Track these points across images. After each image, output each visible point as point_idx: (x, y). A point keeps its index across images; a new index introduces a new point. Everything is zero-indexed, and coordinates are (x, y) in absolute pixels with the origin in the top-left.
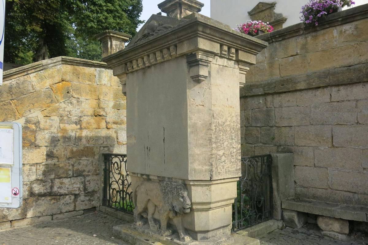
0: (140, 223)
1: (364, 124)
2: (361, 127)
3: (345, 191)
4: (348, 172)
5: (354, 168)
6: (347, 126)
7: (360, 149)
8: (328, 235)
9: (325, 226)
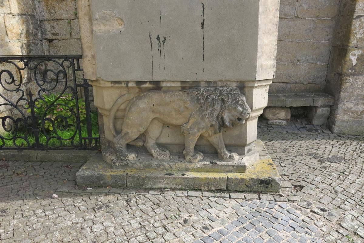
0: (133, 155)
1: (302, 18)
2: (299, 20)
3: (280, 83)
4: (284, 65)
5: (289, 60)
6: (287, 20)
7: (296, 42)
8: (275, 123)
9: (273, 116)
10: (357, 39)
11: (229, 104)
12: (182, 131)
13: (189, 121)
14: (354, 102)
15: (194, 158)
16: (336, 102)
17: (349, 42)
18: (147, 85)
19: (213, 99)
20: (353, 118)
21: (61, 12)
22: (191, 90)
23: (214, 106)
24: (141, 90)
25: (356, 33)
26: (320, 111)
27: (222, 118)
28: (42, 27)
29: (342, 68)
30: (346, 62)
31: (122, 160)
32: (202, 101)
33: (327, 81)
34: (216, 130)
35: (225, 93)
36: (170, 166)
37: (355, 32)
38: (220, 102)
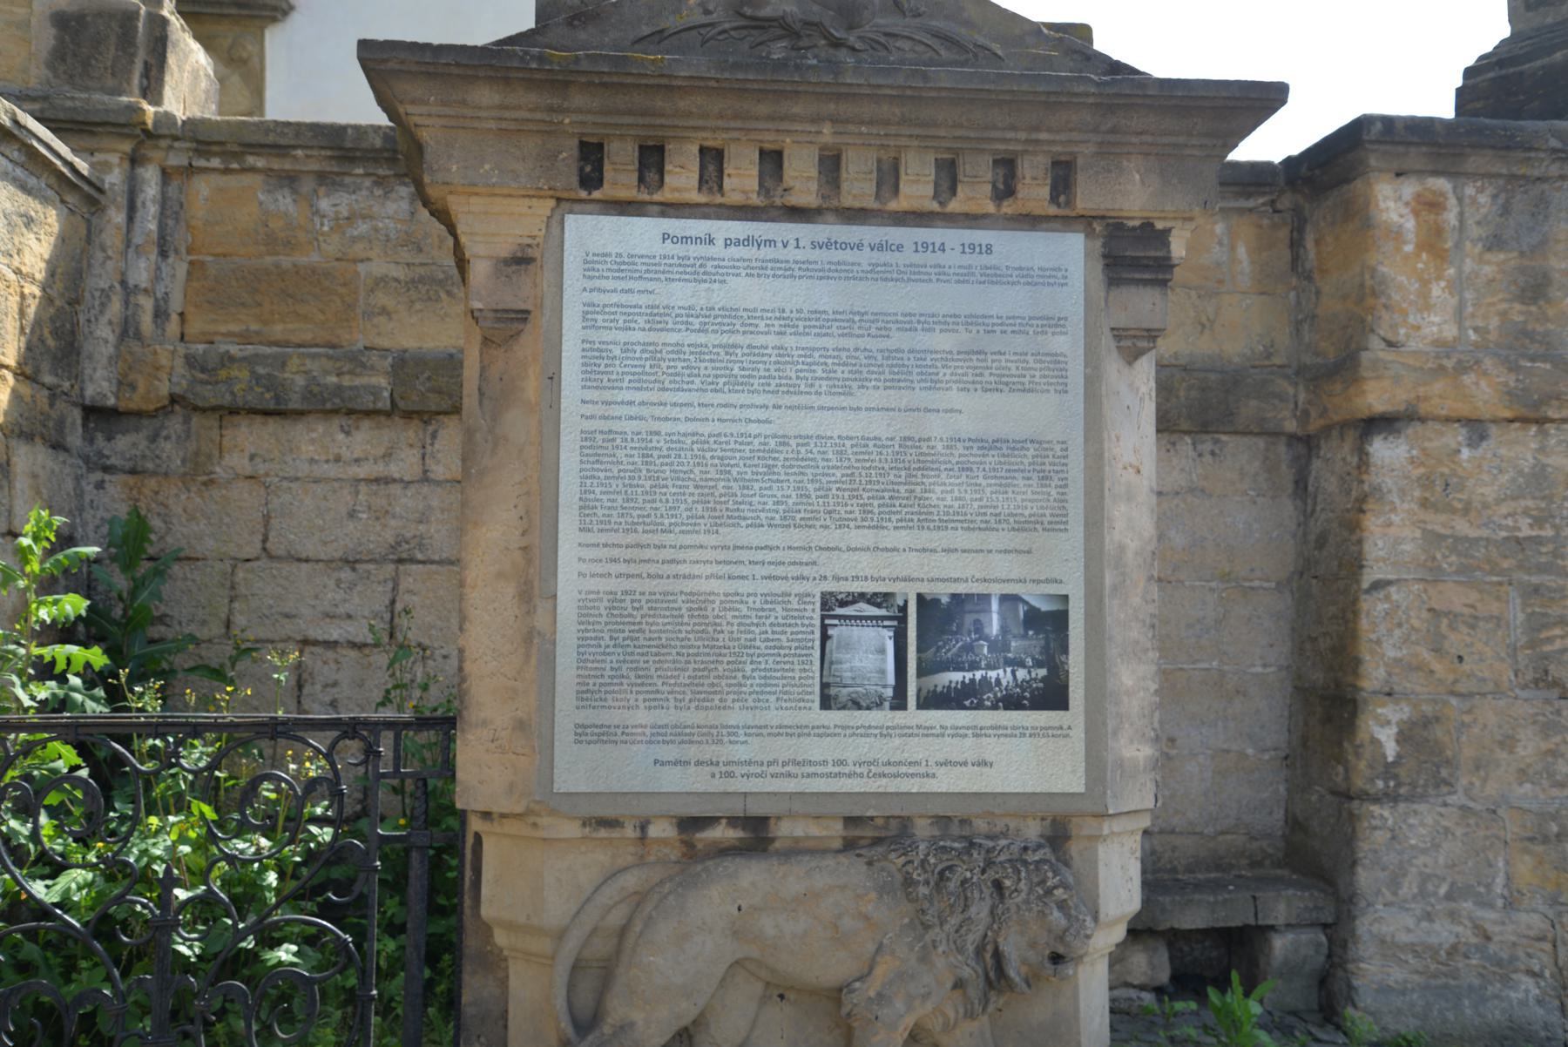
10: (1386, 665)
11: (1019, 900)
12: (845, 1010)
13: (871, 969)
14: (1417, 908)
17: (1355, 673)
18: (721, 833)
19: (964, 882)
20: (1421, 973)
21: (196, 528)
22: (881, 849)
23: (966, 908)
24: (691, 853)
25: (1378, 642)
26: (1280, 944)
27: (997, 955)
28: (95, 589)
29: (1347, 770)
30: (1361, 750)
32: (923, 890)
33: (1295, 824)
34: (972, 1004)
37: (1373, 637)
38: (987, 892)
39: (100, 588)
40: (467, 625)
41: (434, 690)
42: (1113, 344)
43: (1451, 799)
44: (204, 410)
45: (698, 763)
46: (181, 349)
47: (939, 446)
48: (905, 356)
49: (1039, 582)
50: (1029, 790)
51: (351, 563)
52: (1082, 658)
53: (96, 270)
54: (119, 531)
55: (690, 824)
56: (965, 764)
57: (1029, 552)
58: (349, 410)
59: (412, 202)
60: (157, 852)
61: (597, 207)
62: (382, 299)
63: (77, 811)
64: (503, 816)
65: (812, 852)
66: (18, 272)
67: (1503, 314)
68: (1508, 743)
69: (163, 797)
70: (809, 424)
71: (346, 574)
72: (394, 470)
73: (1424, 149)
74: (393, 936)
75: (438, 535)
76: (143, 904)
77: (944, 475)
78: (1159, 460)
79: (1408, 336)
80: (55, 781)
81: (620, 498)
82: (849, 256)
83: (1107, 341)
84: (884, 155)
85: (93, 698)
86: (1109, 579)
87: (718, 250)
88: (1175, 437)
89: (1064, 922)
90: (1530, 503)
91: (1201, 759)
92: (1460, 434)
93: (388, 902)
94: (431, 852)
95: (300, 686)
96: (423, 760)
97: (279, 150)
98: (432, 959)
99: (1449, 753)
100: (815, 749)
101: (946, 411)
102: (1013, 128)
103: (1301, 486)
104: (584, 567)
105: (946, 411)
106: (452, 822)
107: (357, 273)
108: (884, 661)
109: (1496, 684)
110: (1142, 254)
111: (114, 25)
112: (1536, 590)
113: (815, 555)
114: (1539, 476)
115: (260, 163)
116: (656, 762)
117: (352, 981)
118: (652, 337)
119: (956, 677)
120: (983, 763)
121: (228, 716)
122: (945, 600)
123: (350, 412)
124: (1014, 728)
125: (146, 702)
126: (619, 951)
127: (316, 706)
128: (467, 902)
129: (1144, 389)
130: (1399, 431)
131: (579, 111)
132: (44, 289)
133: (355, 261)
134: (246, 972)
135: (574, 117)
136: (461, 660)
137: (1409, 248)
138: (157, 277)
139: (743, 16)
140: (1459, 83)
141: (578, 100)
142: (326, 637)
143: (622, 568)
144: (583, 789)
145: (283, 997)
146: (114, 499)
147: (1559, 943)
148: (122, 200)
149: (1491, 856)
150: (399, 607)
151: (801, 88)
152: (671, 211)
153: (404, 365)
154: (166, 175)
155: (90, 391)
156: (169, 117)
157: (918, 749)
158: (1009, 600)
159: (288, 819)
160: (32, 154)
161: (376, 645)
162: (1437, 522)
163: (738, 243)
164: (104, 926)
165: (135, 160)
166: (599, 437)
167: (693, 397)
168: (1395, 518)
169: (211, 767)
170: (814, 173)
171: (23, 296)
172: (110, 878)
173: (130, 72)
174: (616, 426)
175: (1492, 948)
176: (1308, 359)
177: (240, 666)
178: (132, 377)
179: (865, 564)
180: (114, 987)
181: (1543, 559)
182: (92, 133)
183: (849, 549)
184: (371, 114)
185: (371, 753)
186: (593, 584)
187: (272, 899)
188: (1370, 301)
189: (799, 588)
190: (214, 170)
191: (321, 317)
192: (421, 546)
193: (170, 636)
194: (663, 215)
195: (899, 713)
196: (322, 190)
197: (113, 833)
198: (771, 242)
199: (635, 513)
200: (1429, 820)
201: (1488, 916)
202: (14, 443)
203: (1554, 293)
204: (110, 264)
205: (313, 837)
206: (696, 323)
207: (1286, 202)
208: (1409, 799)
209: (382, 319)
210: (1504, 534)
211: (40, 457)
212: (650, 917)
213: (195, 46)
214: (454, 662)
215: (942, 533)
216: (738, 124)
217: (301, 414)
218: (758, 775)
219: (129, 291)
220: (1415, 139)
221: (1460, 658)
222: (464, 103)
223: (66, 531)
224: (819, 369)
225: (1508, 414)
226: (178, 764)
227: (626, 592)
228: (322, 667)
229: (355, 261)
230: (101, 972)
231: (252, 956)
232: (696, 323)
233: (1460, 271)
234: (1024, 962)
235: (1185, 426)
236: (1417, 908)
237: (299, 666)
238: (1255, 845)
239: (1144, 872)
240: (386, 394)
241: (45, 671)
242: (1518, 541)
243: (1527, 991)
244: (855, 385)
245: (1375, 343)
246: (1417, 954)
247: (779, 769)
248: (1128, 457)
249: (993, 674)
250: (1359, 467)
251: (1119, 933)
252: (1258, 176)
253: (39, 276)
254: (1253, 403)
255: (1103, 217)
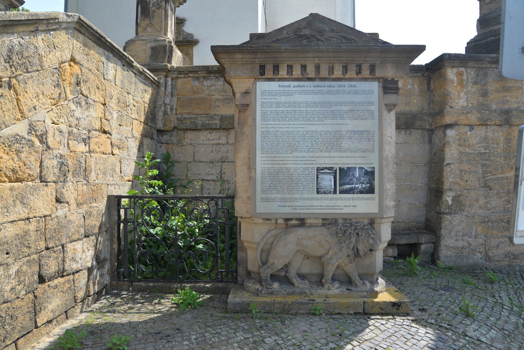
10: (450, 183)
12: (322, 261)
15: (332, 286)
16: (438, 239)
17: (442, 185)
18: (294, 222)
19: (350, 233)
22: (330, 226)
23: (350, 239)
24: (287, 226)
25: (448, 178)
26: (423, 247)
27: (357, 249)
29: (440, 207)
31: (267, 288)
33: (427, 220)
35: (359, 228)
36: (312, 293)
37: (447, 176)
38: (355, 235)
39: (161, 169)
40: (236, 176)
41: (230, 190)
42: (385, 108)
43: (463, 214)
44: (181, 130)
45: (289, 206)
46: (176, 117)
47: (344, 133)
48: (336, 112)
49: (368, 164)
50: (365, 212)
51: (212, 162)
52: (378, 182)
53: (159, 101)
54: (164, 156)
55: (287, 220)
56: (350, 206)
57: (365, 157)
58: (211, 129)
59: (224, 82)
60: (174, 224)
61: (264, 80)
62: (217, 104)
63: (158, 215)
64: (245, 218)
65: (315, 226)
66: (144, 102)
67: (477, 100)
68: (477, 200)
69: (175, 213)
70: (313, 128)
71: (211, 165)
72: (221, 142)
73: (458, 61)
74: (223, 244)
75: (230, 155)
76: (172, 235)
77: (345, 139)
78: (396, 136)
79: (455, 105)
80: (154, 209)
81: (270, 146)
82: (322, 89)
83: (384, 107)
84: (330, 65)
85: (160, 192)
86: (384, 163)
87: (292, 88)
88: (400, 130)
89: (373, 242)
90: (484, 144)
91: (406, 205)
92: (468, 128)
93: (222, 236)
94: (230, 226)
95: (202, 190)
96: (228, 206)
97: (195, 72)
98: (231, 248)
99: (464, 203)
100: (315, 203)
101: (346, 124)
102: (360, 57)
103: (430, 141)
104: (262, 162)
105: (346, 124)
106: (235, 219)
107: (212, 98)
108: (331, 183)
109: (475, 187)
110: (391, 86)
111: (162, 48)
112: (485, 165)
113: (315, 159)
114: (486, 138)
115: (192, 75)
116: (279, 206)
117: (215, 253)
118: (277, 109)
119: (348, 186)
120: (354, 206)
121: (187, 196)
122: (345, 169)
123: (211, 129)
124: (362, 198)
125: (170, 192)
126: (271, 248)
127: (205, 194)
128: (238, 236)
129: (392, 118)
130: (453, 128)
131: (259, 58)
132: (149, 105)
133: (211, 95)
134: (193, 249)
135: (258, 60)
136: (235, 183)
137: (455, 84)
138: (171, 101)
139: (297, 35)
140: (466, 46)
141: (259, 56)
142: (207, 179)
143: (270, 162)
144: (263, 212)
145: (200, 255)
146: (163, 150)
147: (486, 246)
148: (164, 85)
149: (472, 226)
150: (222, 172)
151: (310, 50)
152: (281, 80)
153: (223, 118)
154: (172, 79)
155: (158, 127)
156: (173, 67)
157: (339, 203)
158: (361, 168)
159: (200, 218)
160: (146, 77)
161: (218, 181)
162: (462, 149)
163: (296, 87)
164: (165, 239)
165: (166, 77)
166: (265, 132)
167: (287, 123)
168: (452, 149)
169: (184, 206)
170: (314, 70)
171: (145, 107)
172: (165, 229)
173: (165, 58)
174: (269, 130)
175: (471, 247)
176: (432, 111)
177: (189, 185)
178: (166, 123)
179: (327, 160)
180: (167, 251)
181: (486, 158)
182: (158, 71)
183: (323, 157)
184: (215, 63)
185: (217, 204)
186: (264, 166)
187: (197, 234)
188: (446, 97)
189: (311, 166)
190: (182, 77)
191: (205, 108)
192: (227, 159)
193: (175, 179)
194: (279, 81)
195: (335, 195)
196: (204, 80)
197: (165, 220)
198: (304, 86)
199: (273, 150)
200: (458, 219)
201: (471, 240)
202: (143, 138)
203: (489, 95)
204: (161, 99)
205: (205, 222)
206: (287, 105)
207: (426, 74)
208: (454, 214)
209: (217, 108)
210: (477, 152)
211: (149, 141)
212: (278, 240)
213: (178, 51)
214: (234, 184)
215: (345, 153)
216: (296, 59)
217: (201, 130)
218: (302, 209)
219: (165, 104)
220: (456, 59)
221: (467, 181)
222: (234, 58)
223: (154, 156)
224: (315, 115)
225: (479, 123)
226: (177, 206)
227: (272, 168)
228: (206, 185)
229: (211, 95)
230: (164, 248)
231: (194, 247)
232: (287, 105)
233: (467, 90)
234: (363, 251)
235: (402, 128)
236: (455, 238)
237: (202, 185)
238: (418, 225)
239: (392, 231)
240: (219, 125)
241: (151, 186)
242: (481, 153)
243: (478, 256)
244: (324, 119)
245: (448, 107)
246: (454, 249)
247: (307, 208)
248: (389, 134)
249: (357, 186)
250: (444, 137)
251: (386, 245)
252: (419, 68)
253: (148, 102)
254: (419, 122)
255: (382, 78)
